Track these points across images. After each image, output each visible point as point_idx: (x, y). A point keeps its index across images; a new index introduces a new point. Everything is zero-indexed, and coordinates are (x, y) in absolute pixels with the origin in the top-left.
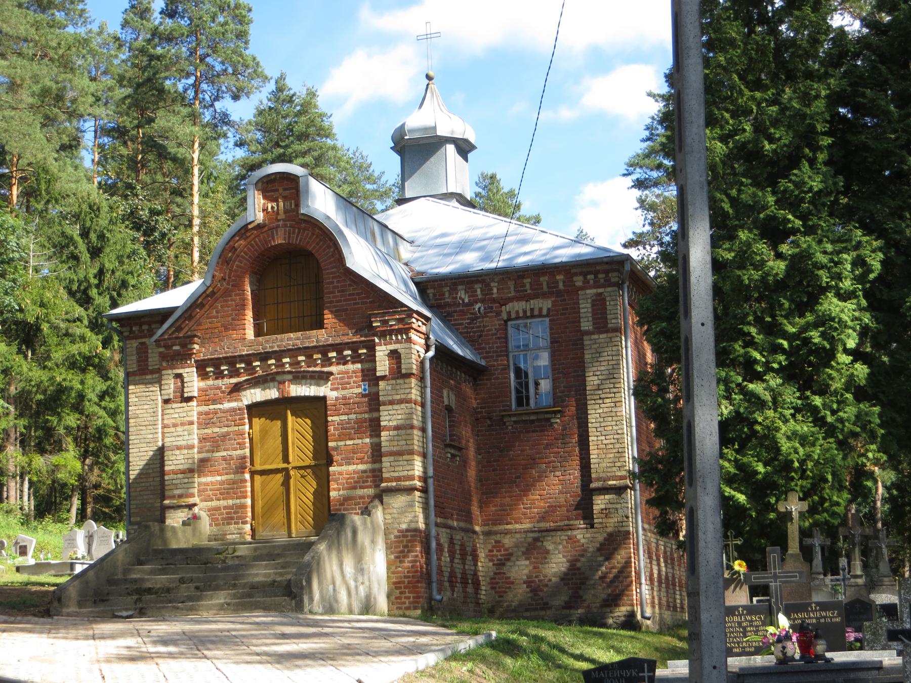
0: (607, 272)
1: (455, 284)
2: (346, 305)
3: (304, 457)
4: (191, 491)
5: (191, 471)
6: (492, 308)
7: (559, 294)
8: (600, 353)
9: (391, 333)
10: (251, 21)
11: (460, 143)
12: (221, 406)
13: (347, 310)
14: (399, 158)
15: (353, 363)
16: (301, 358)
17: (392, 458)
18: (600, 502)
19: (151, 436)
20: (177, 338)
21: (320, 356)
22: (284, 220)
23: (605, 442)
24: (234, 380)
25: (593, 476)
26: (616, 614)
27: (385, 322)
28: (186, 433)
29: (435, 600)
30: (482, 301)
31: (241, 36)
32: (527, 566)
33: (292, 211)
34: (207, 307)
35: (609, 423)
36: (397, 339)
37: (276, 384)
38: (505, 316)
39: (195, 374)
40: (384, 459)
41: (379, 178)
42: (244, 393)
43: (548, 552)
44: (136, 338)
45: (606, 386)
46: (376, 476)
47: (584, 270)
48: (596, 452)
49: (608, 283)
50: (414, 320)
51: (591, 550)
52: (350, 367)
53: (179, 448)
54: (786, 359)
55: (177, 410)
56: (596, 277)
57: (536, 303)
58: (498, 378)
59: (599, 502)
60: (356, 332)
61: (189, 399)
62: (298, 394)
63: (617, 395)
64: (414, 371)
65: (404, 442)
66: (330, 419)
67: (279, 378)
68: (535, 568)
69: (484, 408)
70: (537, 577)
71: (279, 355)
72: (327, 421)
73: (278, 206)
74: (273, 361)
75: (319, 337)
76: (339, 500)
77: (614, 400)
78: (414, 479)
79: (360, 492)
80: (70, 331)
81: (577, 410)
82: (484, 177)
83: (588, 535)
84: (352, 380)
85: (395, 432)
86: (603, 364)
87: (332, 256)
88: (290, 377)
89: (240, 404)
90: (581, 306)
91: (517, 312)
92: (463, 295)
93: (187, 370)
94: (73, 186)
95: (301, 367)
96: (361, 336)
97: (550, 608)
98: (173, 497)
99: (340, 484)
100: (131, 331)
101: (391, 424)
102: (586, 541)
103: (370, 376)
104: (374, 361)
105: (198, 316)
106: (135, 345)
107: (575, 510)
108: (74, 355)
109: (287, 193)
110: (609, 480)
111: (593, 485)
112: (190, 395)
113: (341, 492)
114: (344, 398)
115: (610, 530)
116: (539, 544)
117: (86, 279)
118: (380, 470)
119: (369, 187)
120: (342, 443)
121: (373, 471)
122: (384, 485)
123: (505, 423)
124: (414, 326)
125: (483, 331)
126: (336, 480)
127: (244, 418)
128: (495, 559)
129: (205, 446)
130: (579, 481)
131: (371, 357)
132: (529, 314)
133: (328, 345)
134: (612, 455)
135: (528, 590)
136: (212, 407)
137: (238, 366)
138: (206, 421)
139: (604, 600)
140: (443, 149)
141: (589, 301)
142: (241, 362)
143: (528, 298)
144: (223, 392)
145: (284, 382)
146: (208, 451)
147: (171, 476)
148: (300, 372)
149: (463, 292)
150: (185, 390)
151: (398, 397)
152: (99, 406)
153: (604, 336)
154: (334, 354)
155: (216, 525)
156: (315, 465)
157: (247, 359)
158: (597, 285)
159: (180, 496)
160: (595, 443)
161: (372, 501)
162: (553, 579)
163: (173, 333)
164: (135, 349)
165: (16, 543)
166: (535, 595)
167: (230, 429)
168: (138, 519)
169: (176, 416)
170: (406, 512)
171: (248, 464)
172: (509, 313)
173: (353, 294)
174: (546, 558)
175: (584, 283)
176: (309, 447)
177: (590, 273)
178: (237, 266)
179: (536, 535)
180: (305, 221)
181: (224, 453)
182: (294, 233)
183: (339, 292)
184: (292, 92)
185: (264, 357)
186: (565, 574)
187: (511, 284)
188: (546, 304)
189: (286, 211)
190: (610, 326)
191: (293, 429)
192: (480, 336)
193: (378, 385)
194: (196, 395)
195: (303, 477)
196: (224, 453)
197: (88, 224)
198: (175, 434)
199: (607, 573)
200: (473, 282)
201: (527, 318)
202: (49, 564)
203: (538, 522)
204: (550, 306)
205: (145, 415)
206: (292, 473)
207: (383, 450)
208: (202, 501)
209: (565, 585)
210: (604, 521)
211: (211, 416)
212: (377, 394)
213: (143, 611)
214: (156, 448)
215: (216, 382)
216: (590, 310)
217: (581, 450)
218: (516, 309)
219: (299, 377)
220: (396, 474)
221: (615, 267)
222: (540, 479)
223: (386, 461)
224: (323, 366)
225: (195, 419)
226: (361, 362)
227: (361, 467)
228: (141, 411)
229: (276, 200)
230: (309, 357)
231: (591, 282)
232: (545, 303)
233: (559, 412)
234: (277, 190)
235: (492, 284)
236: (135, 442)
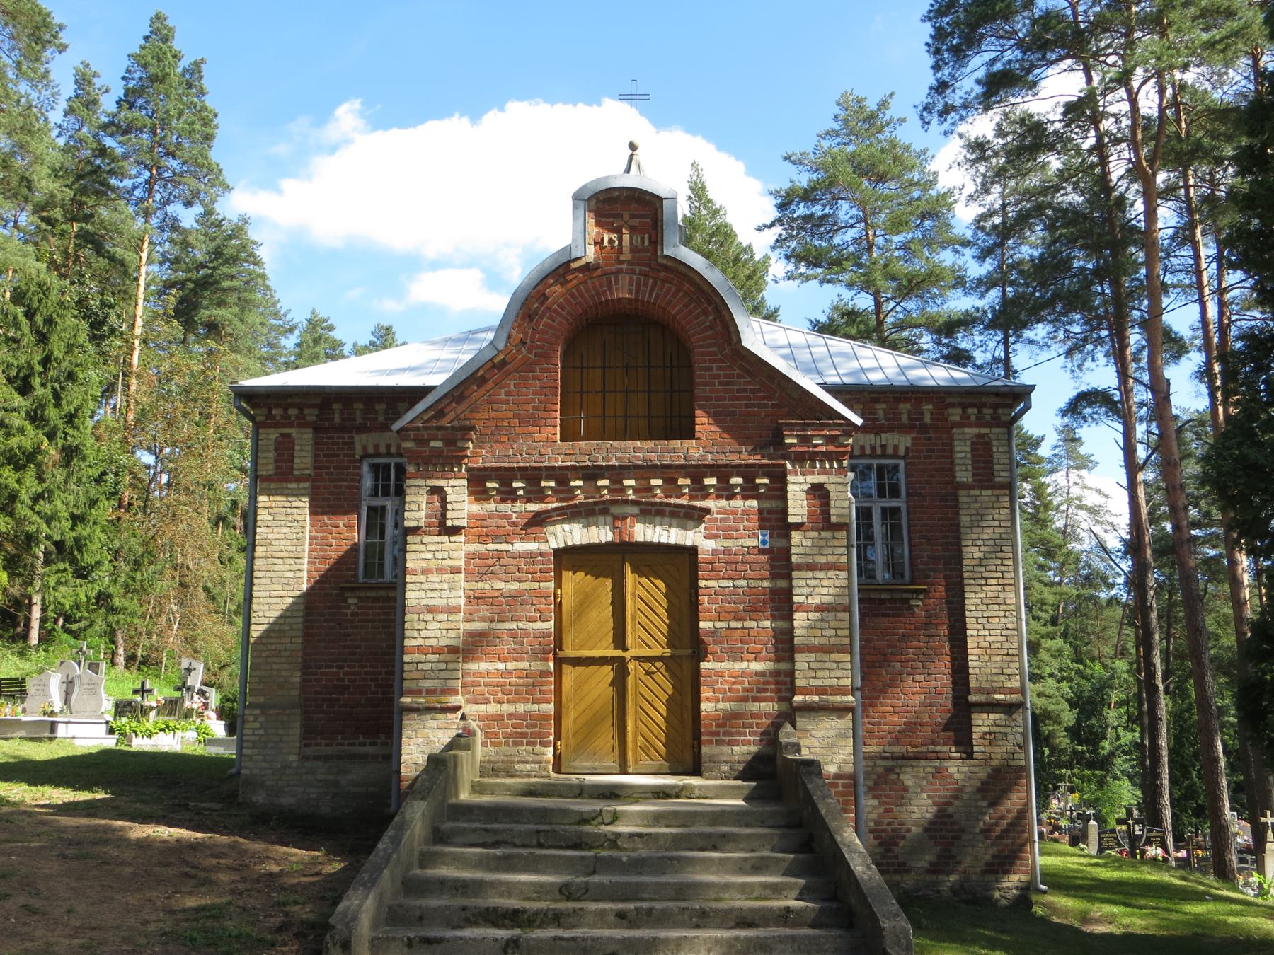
3: (651, 642)
4: (452, 684)
5: (453, 650)
7: (923, 429)
8: (982, 515)
9: (813, 456)
10: (216, 127)
12: (508, 547)
13: (733, 413)
15: (745, 498)
16: (656, 482)
17: (812, 657)
18: (982, 724)
19: (291, 575)
20: (439, 428)
21: (688, 481)
22: (629, 263)
23: (989, 639)
24: (534, 507)
25: (972, 685)
26: (1004, 885)
27: (805, 440)
28: (446, 586)
31: (208, 138)
32: (874, 807)
33: (644, 250)
35: (995, 614)
36: (823, 467)
37: (609, 519)
40: (798, 657)
41: (285, 315)
42: (550, 529)
43: (906, 789)
44: (276, 426)
45: (991, 562)
46: (784, 683)
47: (964, 400)
48: (976, 651)
51: (968, 790)
52: (738, 503)
53: (432, 610)
55: (430, 547)
56: (980, 412)
59: (981, 723)
60: (754, 450)
61: (455, 530)
62: (648, 539)
65: (832, 632)
66: (702, 583)
67: (615, 510)
68: (886, 811)
70: (889, 824)
71: (617, 473)
73: (620, 239)
74: (606, 482)
76: (716, 718)
77: (1001, 581)
79: (754, 707)
80: (7, 421)
81: (947, 591)
82: (380, 327)
83: (965, 769)
84: (741, 526)
85: (817, 615)
86: (986, 530)
87: (711, 327)
88: (636, 510)
89: (544, 547)
91: (862, 448)
93: (452, 482)
94: (20, 259)
95: (655, 496)
96: (763, 457)
97: (908, 871)
98: (417, 692)
99: (719, 691)
100: (269, 415)
101: (810, 600)
102: (962, 776)
104: (784, 498)
105: (473, 397)
106: (273, 437)
107: (944, 730)
108: (12, 449)
109: (636, 222)
110: (995, 692)
111: (973, 698)
112: (456, 523)
113: (721, 705)
114: (727, 552)
115: (995, 763)
116: (893, 777)
117: (30, 367)
118: (791, 674)
119: (274, 322)
121: (776, 673)
122: (798, 698)
126: (712, 686)
129: (479, 611)
130: (950, 690)
132: (879, 452)
133: (705, 466)
134: (999, 658)
135: (876, 842)
136: (492, 547)
137: (543, 484)
138: (481, 568)
139: (987, 864)
141: (968, 443)
142: (548, 478)
144: (514, 524)
145: (625, 518)
147: (416, 657)
150: (449, 515)
151: (823, 559)
152: (32, 508)
153: (989, 492)
155: (493, 744)
156: (671, 657)
157: (562, 476)
158: (980, 423)
159: (431, 692)
160: (975, 639)
162: (913, 829)
163: (429, 420)
164: (272, 442)
166: (888, 851)
167: (524, 586)
168: (262, 700)
169: (430, 556)
170: (833, 745)
173: (745, 390)
175: (962, 418)
176: (660, 623)
177: (972, 405)
178: (546, 325)
179: (889, 763)
180: (666, 268)
181: (513, 625)
182: (646, 285)
183: (720, 383)
184: (220, 217)
186: (931, 822)
189: (633, 250)
190: (997, 479)
191: (633, 594)
193: (789, 538)
194: (464, 523)
195: (648, 673)
196: (513, 625)
197: (35, 305)
198: (425, 586)
199: (992, 825)
202: (18, 721)
203: (890, 744)
204: (909, 444)
205: (283, 542)
206: (631, 666)
207: (796, 641)
208: (468, 702)
209: (930, 838)
210: (988, 749)
211: (491, 561)
212: (787, 551)
214: (298, 593)
215: (502, 507)
216: (969, 455)
217: (952, 647)
218: (861, 443)
219: (651, 512)
220: (818, 683)
222: (892, 683)
223: (802, 662)
224: (691, 498)
225: (462, 563)
226: (758, 497)
227: (756, 666)
228: (277, 536)
229: (618, 231)
230: (670, 481)
231: (973, 418)
232: (903, 439)
234: (621, 216)
236: (263, 581)
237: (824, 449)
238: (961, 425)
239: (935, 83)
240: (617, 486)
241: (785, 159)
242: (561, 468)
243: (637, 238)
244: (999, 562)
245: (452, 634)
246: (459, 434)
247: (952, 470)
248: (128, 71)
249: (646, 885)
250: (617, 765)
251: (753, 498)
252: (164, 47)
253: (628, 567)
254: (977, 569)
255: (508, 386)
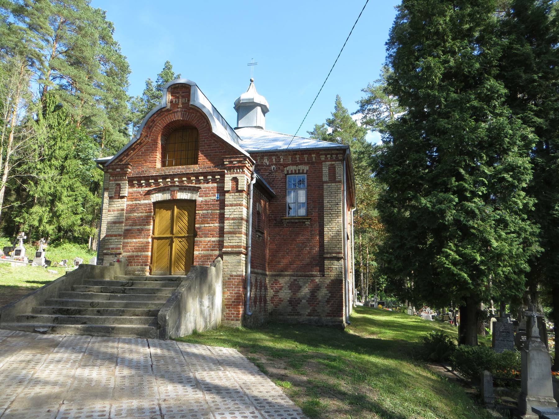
0: (337, 154)
1: (263, 156)
2: (211, 153)
6: (280, 168)
9: (234, 168)
11: (263, 107)
12: (139, 202)
13: (211, 155)
14: (236, 113)
15: (212, 183)
16: (184, 179)
17: (230, 235)
20: (119, 165)
23: (332, 235)
24: (147, 189)
25: (325, 251)
27: (231, 162)
29: (248, 315)
30: (276, 165)
33: (186, 103)
34: (137, 150)
35: (334, 226)
36: (237, 171)
38: (286, 172)
39: (127, 185)
42: (152, 196)
46: (221, 244)
49: (337, 160)
50: (247, 162)
52: (210, 185)
54: (486, 190)
56: (331, 156)
57: (301, 167)
58: (281, 201)
61: (123, 197)
63: (339, 213)
64: (245, 189)
66: (197, 212)
67: (171, 189)
68: (294, 294)
69: (273, 215)
71: (172, 176)
72: (195, 213)
74: (169, 180)
75: (195, 168)
77: (337, 215)
78: (241, 247)
88: (178, 188)
90: (323, 169)
91: (292, 171)
92: (266, 161)
93: (123, 182)
95: (184, 184)
103: (222, 191)
105: (131, 155)
109: (183, 94)
110: (333, 254)
112: (123, 195)
114: (206, 201)
115: (332, 278)
116: (297, 282)
120: (203, 225)
122: (224, 249)
123: (283, 223)
124: (247, 165)
125: (275, 179)
127: (151, 209)
128: (274, 288)
131: (222, 181)
132: (297, 172)
133: (199, 173)
134: (335, 242)
136: (134, 202)
137: (150, 181)
140: (256, 108)
141: (327, 167)
142: (152, 179)
143: (297, 164)
145: (174, 191)
146: (130, 225)
148: (183, 186)
149: (266, 160)
151: (235, 202)
153: (334, 184)
154: (202, 178)
157: (156, 178)
158: (332, 160)
159: (112, 249)
161: (217, 258)
163: (118, 162)
165: (75, 261)
171: (151, 234)
172: (288, 171)
174: (300, 290)
175: (325, 159)
177: (329, 154)
181: (139, 227)
182: (186, 114)
185: (164, 177)
187: (290, 157)
188: (306, 168)
190: (337, 180)
192: (274, 181)
193: (225, 195)
194: (126, 195)
196: (139, 227)
200: (271, 155)
201: (296, 174)
203: (297, 271)
204: (308, 169)
206: (174, 240)
207: (225, 230)
209: (308, 304)
213: (54, 329)
216: (327, 172)
218: (291, 169)
219: (183, 189)
220: (231, 244)
221: (342, 152)
224: (196, 184)
226: (217, 182)
227: (214, 239)
229: (178, 98)
230: (189, 179)
231: (329, 159)
232: (305, 167)
233: (310, 219)
235: (281, 157)
237: (237, 165)
238: (325, 161)
239: (387, 55)
240: (173, 181)
241: (362, 90)
242: (155, 176)
243: (184, 100)
244: (337, 208)
245: (120, 230)
246: (125, 166)
247: (321, 177)
248: (158, 79)
249: (116, 303)
250: (169, 272)
251: (215, 183)
252: (168, 71)
253: (175, 207)
254: (328, 211)
255: (142, 151)
